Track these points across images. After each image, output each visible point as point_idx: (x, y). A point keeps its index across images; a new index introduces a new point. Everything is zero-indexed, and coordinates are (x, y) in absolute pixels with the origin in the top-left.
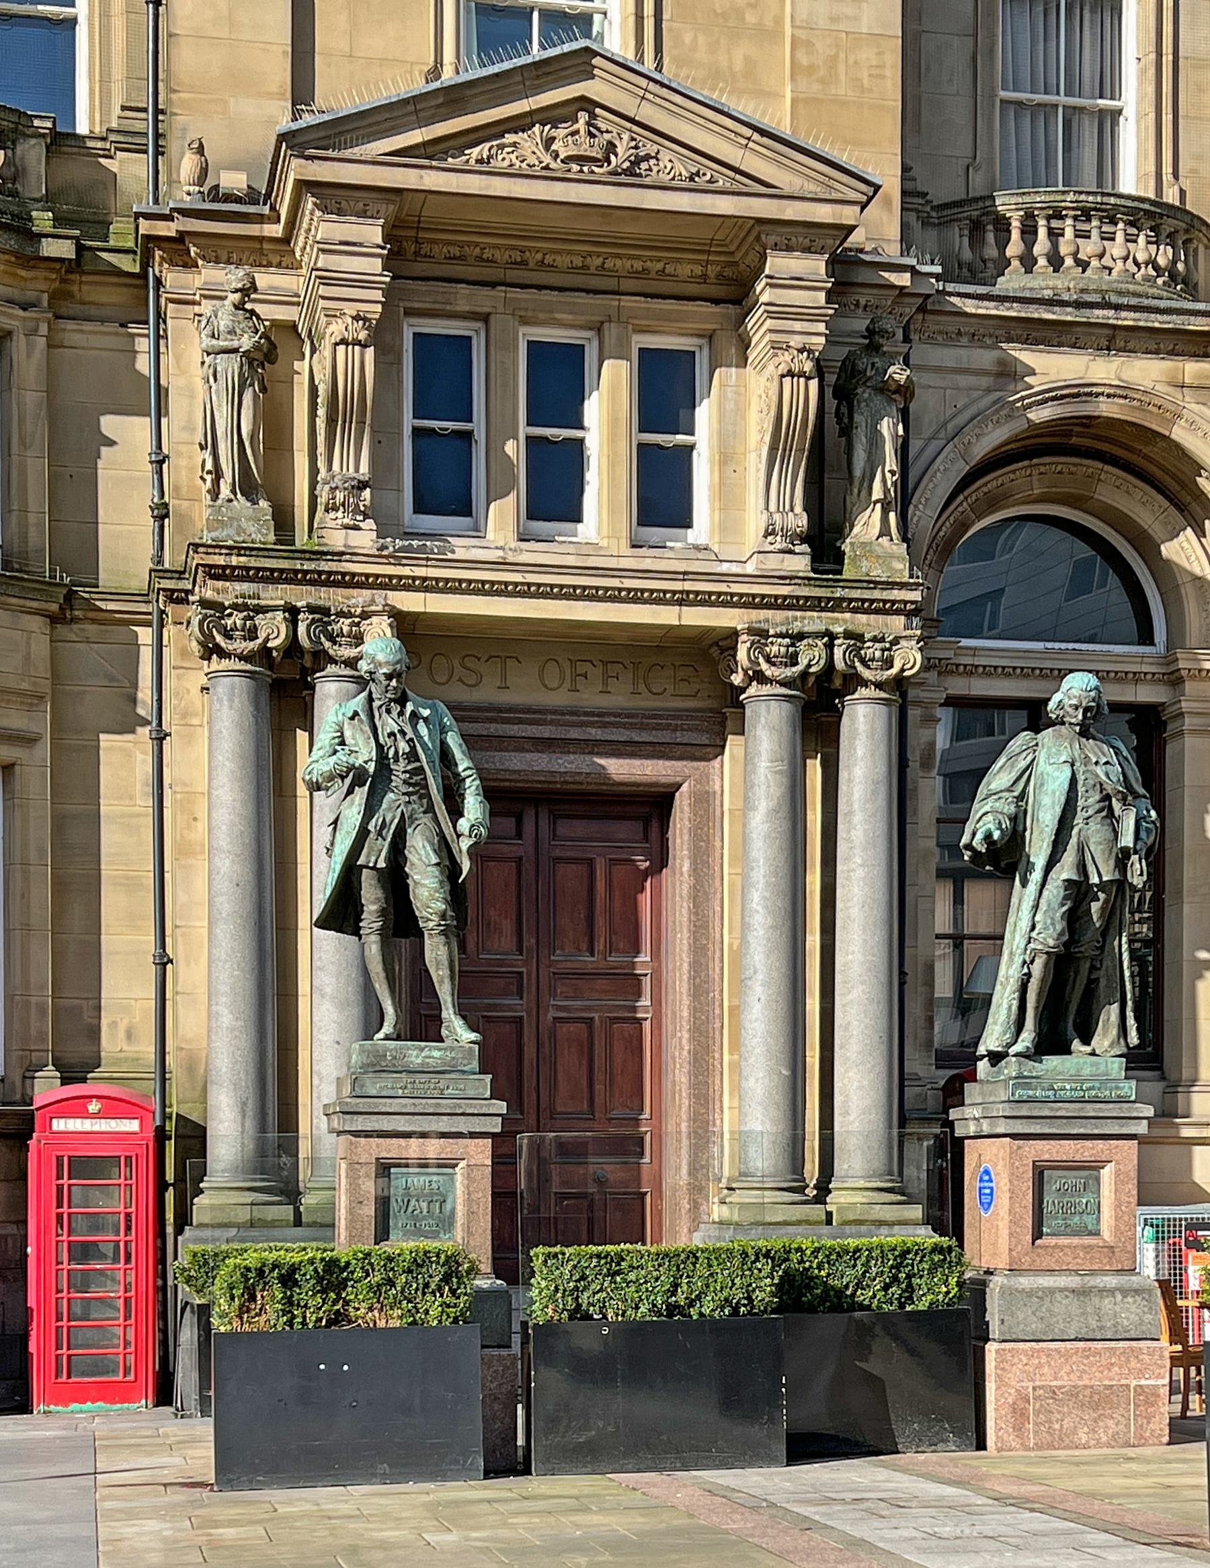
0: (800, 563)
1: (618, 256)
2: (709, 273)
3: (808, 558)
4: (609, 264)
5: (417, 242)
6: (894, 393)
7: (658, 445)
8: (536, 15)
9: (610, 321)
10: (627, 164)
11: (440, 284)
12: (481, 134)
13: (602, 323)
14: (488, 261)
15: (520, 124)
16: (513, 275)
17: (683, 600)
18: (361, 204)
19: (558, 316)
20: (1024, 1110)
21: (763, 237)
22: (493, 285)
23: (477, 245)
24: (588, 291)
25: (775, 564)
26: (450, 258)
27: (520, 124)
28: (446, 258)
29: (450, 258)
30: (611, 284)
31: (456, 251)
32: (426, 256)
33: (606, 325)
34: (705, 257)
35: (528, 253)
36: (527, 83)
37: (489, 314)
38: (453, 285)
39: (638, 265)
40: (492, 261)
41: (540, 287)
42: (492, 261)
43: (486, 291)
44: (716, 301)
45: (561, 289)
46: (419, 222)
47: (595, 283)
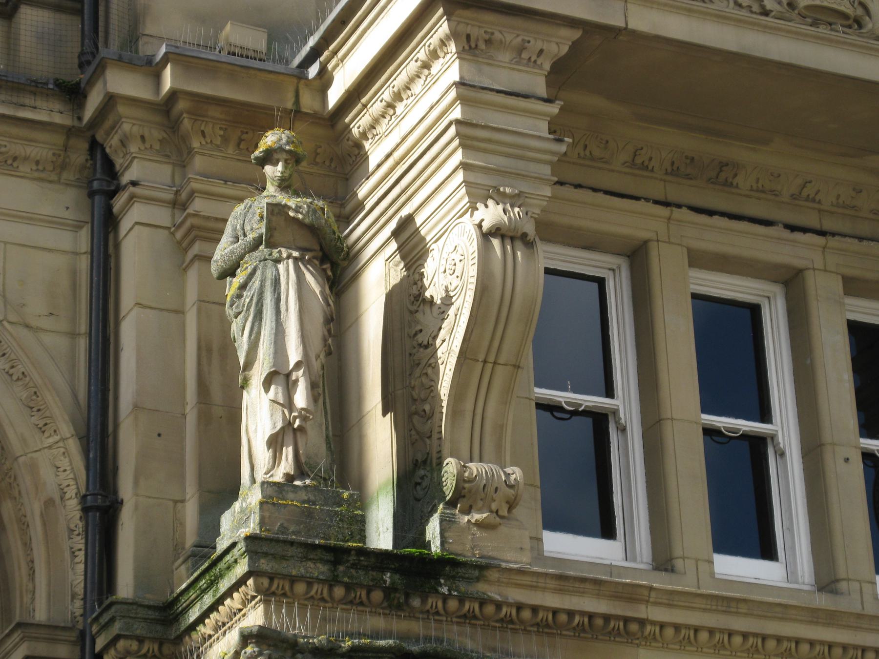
30: (812, 220)
32: (807, 199)
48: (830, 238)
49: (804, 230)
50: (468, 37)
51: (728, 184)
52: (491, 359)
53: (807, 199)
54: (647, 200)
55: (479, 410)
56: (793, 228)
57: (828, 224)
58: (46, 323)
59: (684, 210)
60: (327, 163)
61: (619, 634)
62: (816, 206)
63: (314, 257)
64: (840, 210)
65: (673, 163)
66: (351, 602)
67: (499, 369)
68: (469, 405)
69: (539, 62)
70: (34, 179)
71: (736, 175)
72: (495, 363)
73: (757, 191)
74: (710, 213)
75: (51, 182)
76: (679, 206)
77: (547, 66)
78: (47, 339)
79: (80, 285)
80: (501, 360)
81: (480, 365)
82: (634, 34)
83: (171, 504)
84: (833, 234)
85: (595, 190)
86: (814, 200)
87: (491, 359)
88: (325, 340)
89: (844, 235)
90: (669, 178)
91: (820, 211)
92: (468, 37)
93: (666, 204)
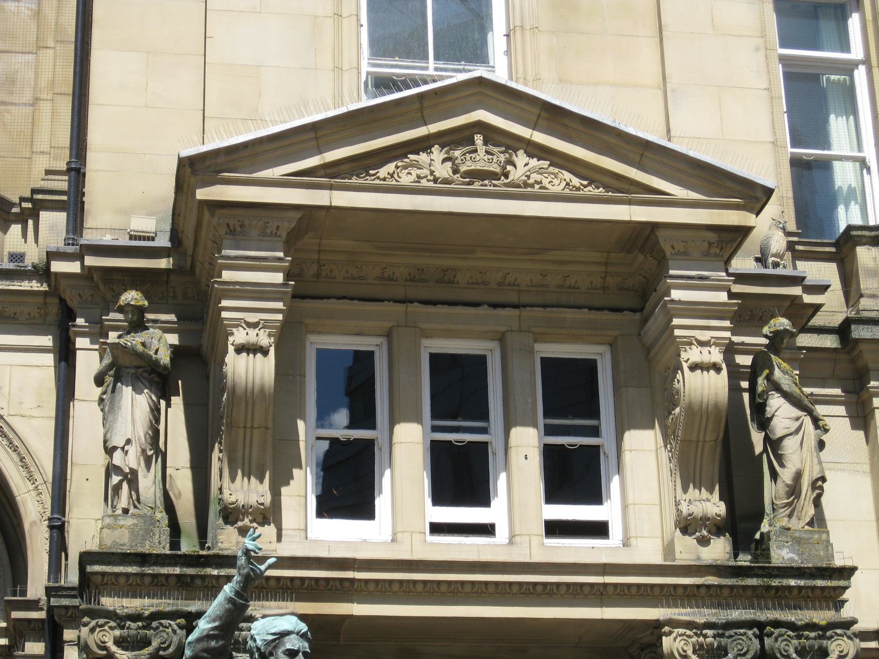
15: (422, 145)
25: (687, 550)
27: (422, 145)
30: (513, 298)
32: (509, 285)
37: (504, 333)
48: (522, 309)
49: (503, 306)
50: (228, 225)
51: (450, 282)
52: (249, 425)
53: (509, 285)
54: (389, 301)
55: (247, 456)
56: (495, 306)
57: (525, 299)
58: (35, 413)
59: (416, 304)
60: (196, 297)
61: (337, 589)
62: (515, 288)
63: (145, 371)
64: (534, 289)
65: (410, 274)
66: (156, 585)
67: (256, 431)
68: (239, 454)
69: (278, 234)
70: (29, 324)
71: (455, 276)
73: (473, 284)
74: (434, 303)
75: (39, 324)
76: (412, 302)
77: (284, 235)
78: (35, 422)
79: (465, 258)
80: (256, 425)
81: (241, 431)
82: (337, 208)
83: (94, 521)
84: (525, 306)
85: (352, 299)
86: (514, 285)
87: (249, 425)
88: (151, 422)
89: (532, 306)
90: (408, 283)
91: (518, 291)
92: (228, 225)
93: (403, 302)
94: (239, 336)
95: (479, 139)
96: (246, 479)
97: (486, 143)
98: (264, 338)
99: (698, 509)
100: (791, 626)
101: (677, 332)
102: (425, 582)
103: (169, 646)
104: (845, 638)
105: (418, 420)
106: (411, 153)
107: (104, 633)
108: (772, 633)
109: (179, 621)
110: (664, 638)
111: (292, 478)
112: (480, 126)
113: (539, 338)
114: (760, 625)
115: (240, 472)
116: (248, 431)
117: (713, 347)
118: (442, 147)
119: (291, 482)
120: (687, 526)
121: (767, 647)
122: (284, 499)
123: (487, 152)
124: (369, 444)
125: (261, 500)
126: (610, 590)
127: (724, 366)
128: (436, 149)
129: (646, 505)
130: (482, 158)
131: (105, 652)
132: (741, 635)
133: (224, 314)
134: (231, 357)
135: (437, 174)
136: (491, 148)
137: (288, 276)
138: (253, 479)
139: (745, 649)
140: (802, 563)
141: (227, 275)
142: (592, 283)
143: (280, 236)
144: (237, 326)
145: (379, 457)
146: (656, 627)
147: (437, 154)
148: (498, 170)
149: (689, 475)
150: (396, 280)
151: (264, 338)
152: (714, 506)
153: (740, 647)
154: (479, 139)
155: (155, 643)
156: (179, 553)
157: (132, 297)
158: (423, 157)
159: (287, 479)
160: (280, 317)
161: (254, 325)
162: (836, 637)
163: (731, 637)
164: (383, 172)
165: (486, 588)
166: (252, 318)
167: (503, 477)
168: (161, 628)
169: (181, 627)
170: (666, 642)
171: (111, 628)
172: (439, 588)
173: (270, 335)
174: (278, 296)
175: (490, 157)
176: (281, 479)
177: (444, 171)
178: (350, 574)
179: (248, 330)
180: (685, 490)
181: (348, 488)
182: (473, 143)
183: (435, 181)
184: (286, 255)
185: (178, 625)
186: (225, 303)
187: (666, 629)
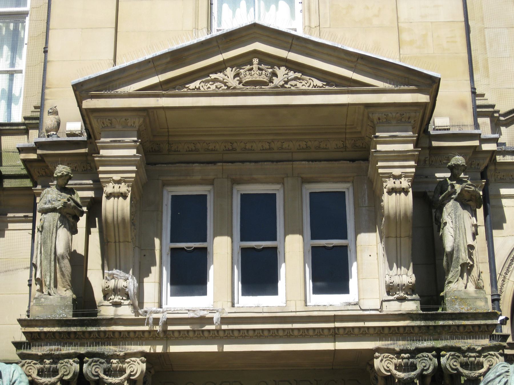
0: (412, 306)
1: (291, 140)
2: (348, 145)
3: (419, 302)
4: (285, 145)
5: (169, 144)
6: (469, 201)
7: (325, 247)
8: (423, 98)
9: (288, 177)
10: (282, 83)
11: (183, 165)
12: (491, 243)
13: (283, 178)
14: (212, 150)
15: (219, 67)
16: (227, 157)
17: (335, 335)
18: (124, 119)
19: (255, 176)
20: (116, 226)
21: (370, 115)
22: (214, 163)
23: (204, 142)
24: (272, 161)
25: (394, 307)
26: (189, 151)
27: (219, 67)
28: (187, 151)
29: (189, 151)
30: (288, 156)
31: (192, 146)
32: (175, 151)
33: (285, 179)
34: (344, 136)
35: (235, 144)
36: (221, 46)
37: (214, 180)
38: (191, 165)
39: (303, 144)
40: (214, 150)
41: (243, 162)
42: (214, 150)
43: (210, 167)
44: (353, 160)
45: (256, 162)
46: (168, 132)
47: (277, 156)
52: (117, 241)
67: (122, 245)
72: (119, 242)
87: (117, 241)
94: (390, 183)
95: (256, 61)
96: (399, 269)
97: (260, 63)
98: (405, 183)
99: (397, 280)
100: (458, 349)
101: (380, 171)
102: (179, 331)
103: (428, 369)
104: (495, 357)
105: (301, 233)
106: (212, 73)
107: (31, 367)
108: (88, 361)
109: (141, 358)
110: (375, 360)
111: (151, 272)
112: (256, 53)
113: (236, 182)
114: (438, 350)
115: (395, 265)
116: (117, 244)
117: (403, 179)
118: (232, 67)
119: (150, 275)
120: (391, 289)
121: (84, 371)
122: (145, 285)
123: (259, 69)
124: (345, 248)
125: (410, 281)
126: (132, 335)
127: (410, 190)
128: (229, 69)
129: (375, 278)
130: (255, 73)
131: (456, 372)
132: (426, 357)
133: (101, 176)
134: (385, 197)
135: (229, 84)
136: (263, 66)
137: (416, 146)
138: (402, 268)
139: (427, 367)
140: (468, 310)
141: (380, 147)
142: (300, 146)
143: (410, 123)
144: (389, 177)
145: (351, 255)
146: (370, 354)
147: (230, 72)
148: (266, 79)
149: (394, 259)
150: (217, 151)
151: (405, 183)
152: (407, 277)
153: (424, 364)
154: (256, 61)
155: (128, 372)
156: (447, 312)
157: (61, 169)
158: (219, 76)
159: (148, 273)
160: (134, 175)
161: (119, 182)
162: (489, 356)
163: (128, 362)
164: (192, 86)
165: (458, 329)
166: (116, 177)
167: (355, 264)
168: (132, 363)
169: (434, 356)
170: (377, 363)
171: (35, 364)
172: (353, 331)
173: (128, 186)
174: (133, 163)
175: (260, 72)
176: (142, 274)
177: (233, 83)
178: (338, 325)
179: (114, 185)
180: (391, 268)
181: (189, 275)
182: (251, 64)
183: (229, 88)
184: (138, 139)
185: (433, 355)
186: (380, 164)
187: (377, 354)
